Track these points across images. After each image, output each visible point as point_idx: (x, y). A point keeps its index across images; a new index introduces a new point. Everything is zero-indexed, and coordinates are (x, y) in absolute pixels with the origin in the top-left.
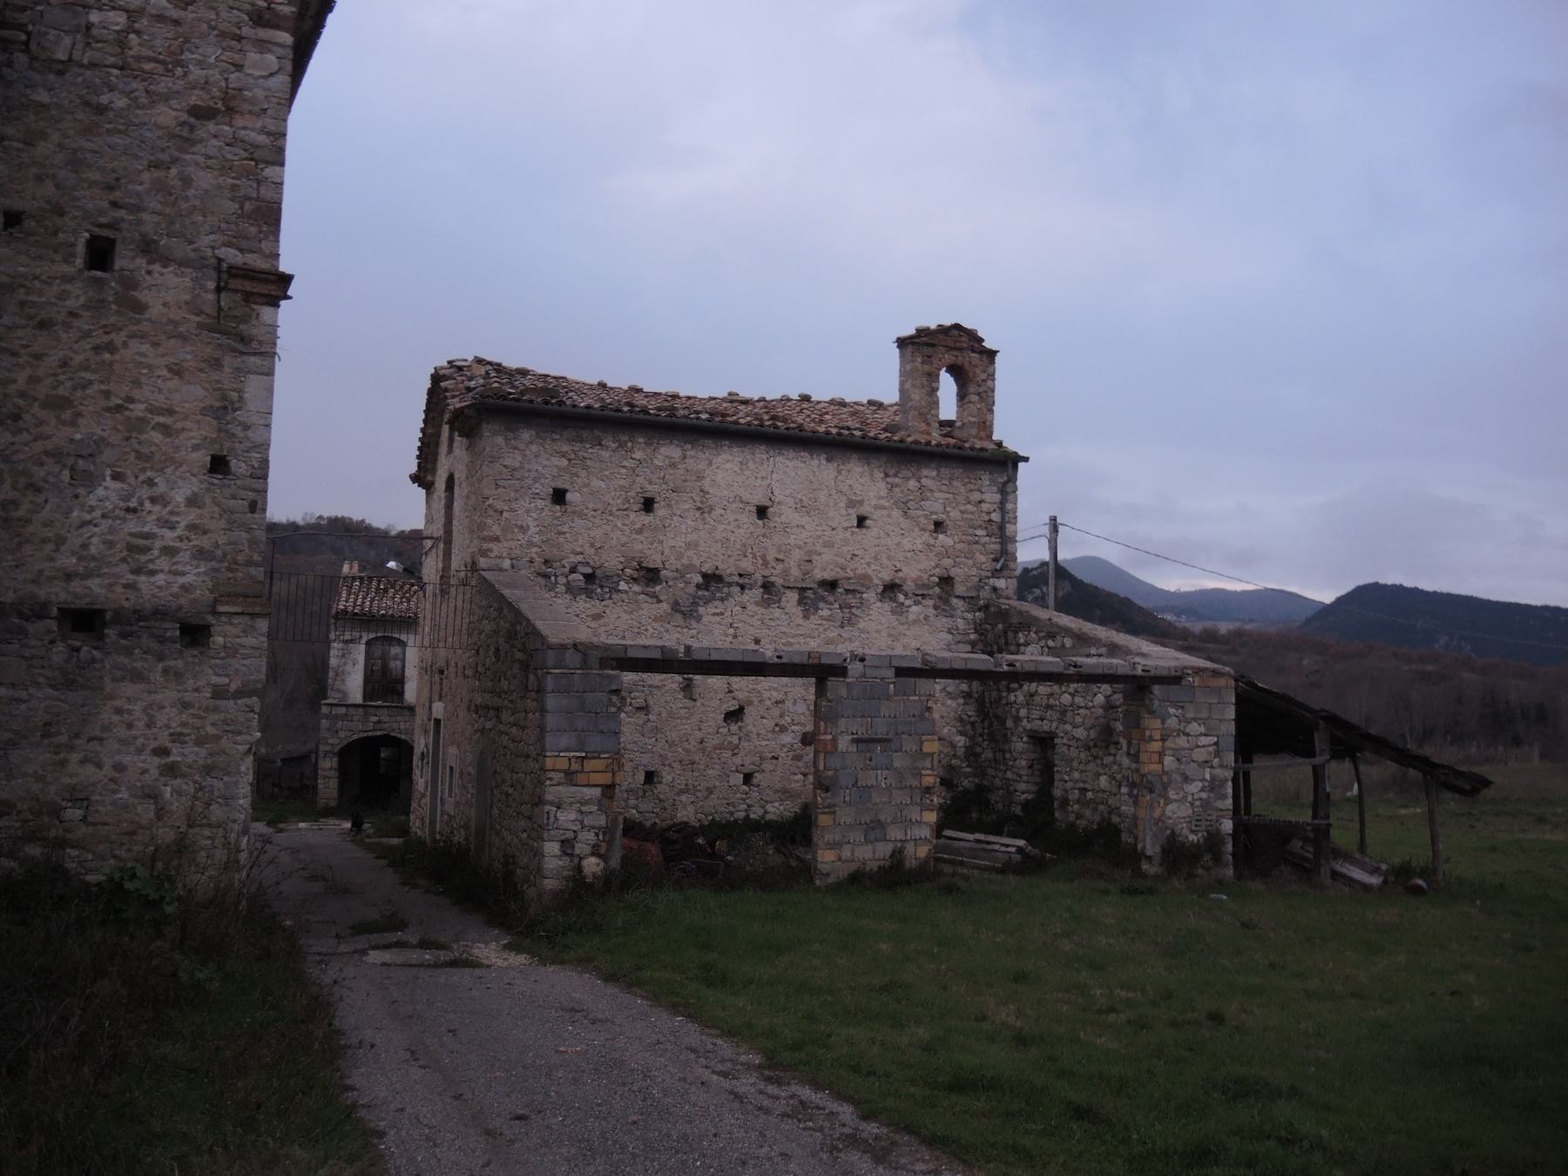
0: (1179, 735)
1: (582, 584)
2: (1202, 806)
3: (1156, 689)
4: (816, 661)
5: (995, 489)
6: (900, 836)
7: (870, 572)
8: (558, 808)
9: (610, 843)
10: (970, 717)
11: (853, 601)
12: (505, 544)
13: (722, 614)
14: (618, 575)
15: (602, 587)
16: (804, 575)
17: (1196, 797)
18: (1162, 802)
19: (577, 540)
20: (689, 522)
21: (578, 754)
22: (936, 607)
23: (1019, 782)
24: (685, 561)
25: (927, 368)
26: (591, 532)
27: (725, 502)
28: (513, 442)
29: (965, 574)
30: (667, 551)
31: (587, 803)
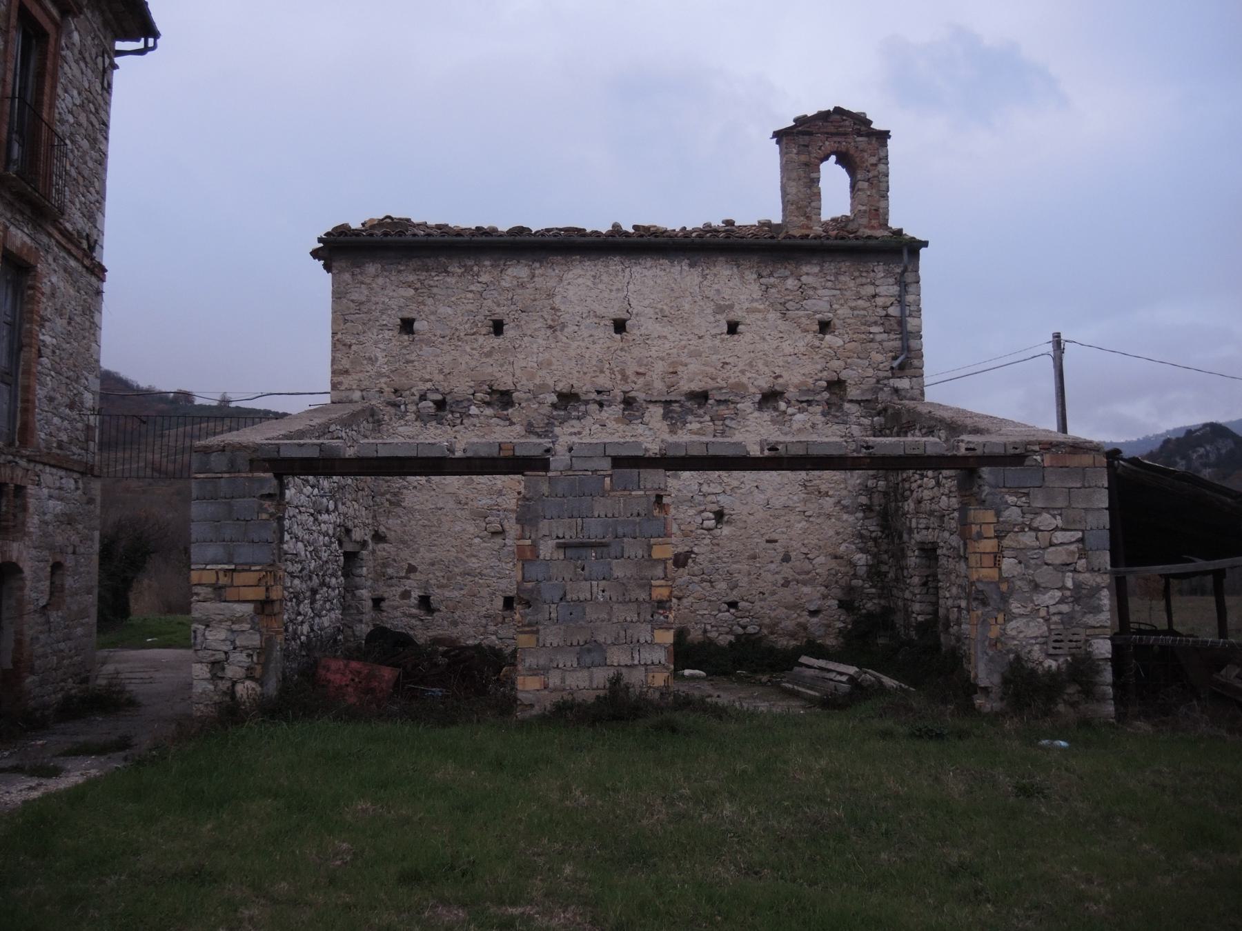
0: (1022, 530)
1: (432, 411)
2: (1062, 623)
3: (985, 472)
4: (510, 453)
5: (892, 280)
6: (625, 660)
7: (744, 380)
8: (207, 626)
9: (265, 666)
10: (872, 532)
11: (727, 412)
12: (356, 377)
13: (580, 433)
14: (469, 400)
15: (452, 412)
16: (669, 387)
17: (1052, 610)
18: (1001, 618)
19: (425, 368)
20: (540, 341)
21: (226, 567)
22: (824, 414)
23: (913, 601)
24: (537, 381)
25: (803, 158)
26: (439, 359)
27: (578, 318)
28: (359, 277)
29: (858, 377)
30: (518, 373)
31: (239, 620)
